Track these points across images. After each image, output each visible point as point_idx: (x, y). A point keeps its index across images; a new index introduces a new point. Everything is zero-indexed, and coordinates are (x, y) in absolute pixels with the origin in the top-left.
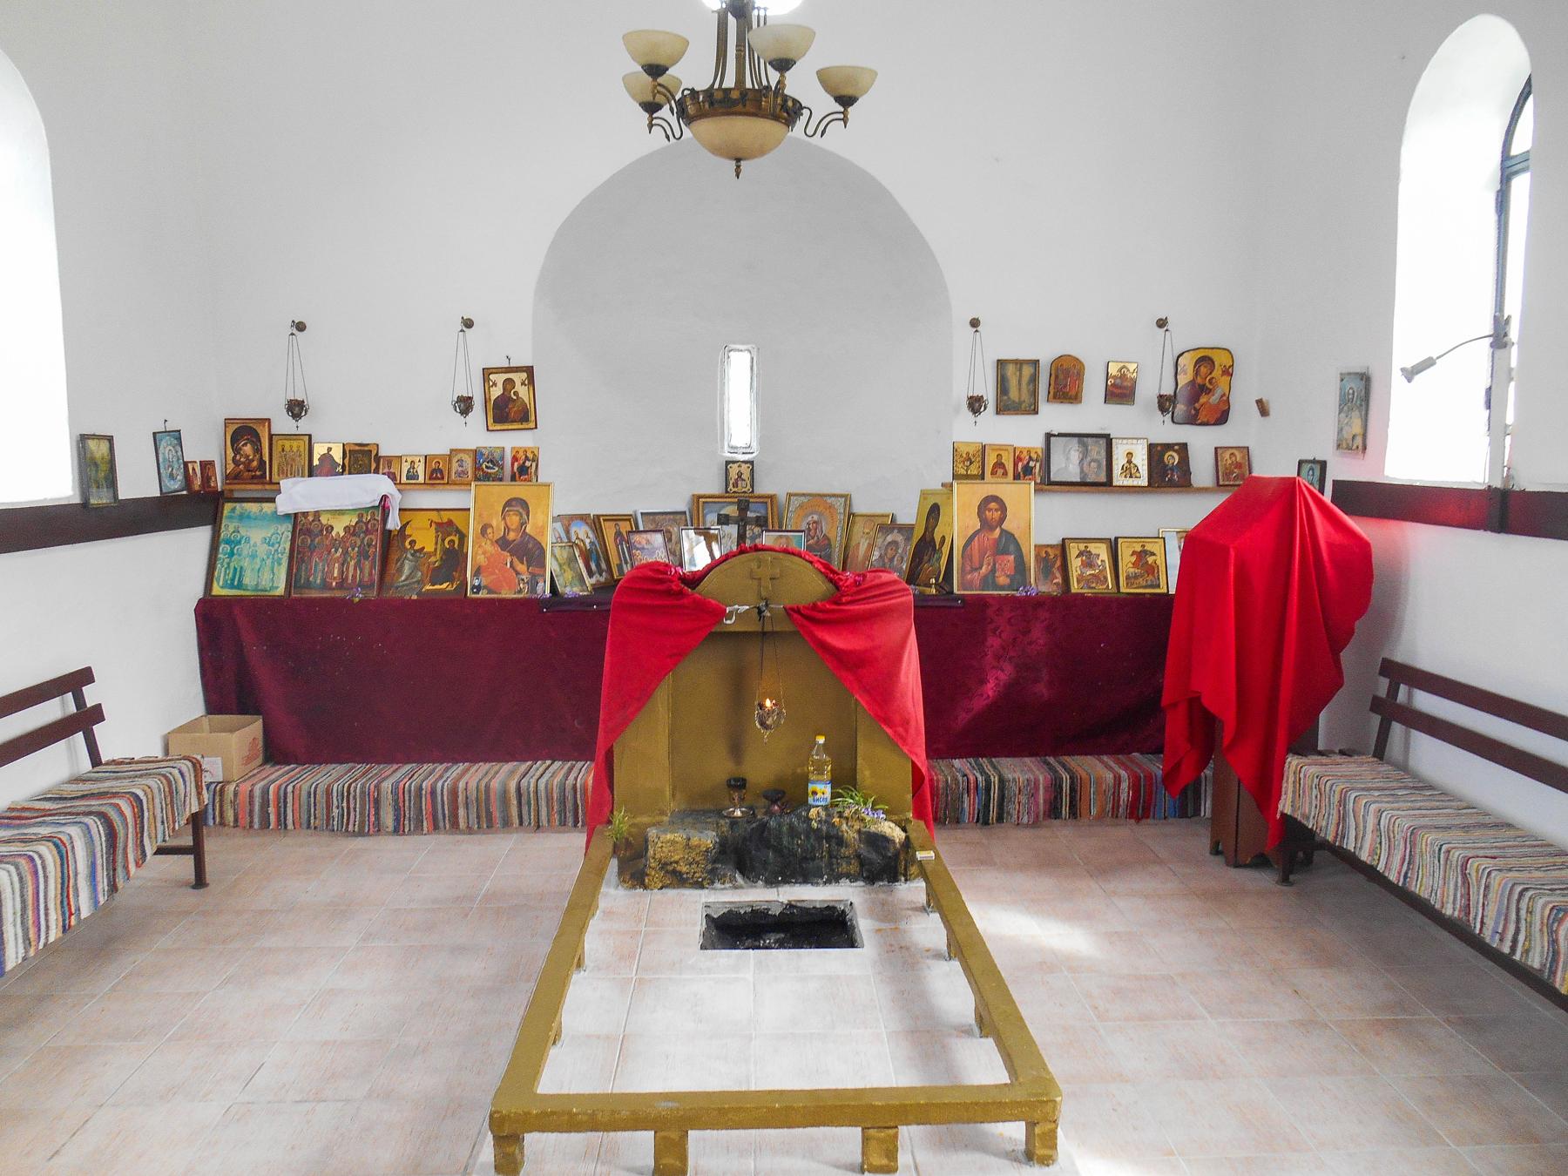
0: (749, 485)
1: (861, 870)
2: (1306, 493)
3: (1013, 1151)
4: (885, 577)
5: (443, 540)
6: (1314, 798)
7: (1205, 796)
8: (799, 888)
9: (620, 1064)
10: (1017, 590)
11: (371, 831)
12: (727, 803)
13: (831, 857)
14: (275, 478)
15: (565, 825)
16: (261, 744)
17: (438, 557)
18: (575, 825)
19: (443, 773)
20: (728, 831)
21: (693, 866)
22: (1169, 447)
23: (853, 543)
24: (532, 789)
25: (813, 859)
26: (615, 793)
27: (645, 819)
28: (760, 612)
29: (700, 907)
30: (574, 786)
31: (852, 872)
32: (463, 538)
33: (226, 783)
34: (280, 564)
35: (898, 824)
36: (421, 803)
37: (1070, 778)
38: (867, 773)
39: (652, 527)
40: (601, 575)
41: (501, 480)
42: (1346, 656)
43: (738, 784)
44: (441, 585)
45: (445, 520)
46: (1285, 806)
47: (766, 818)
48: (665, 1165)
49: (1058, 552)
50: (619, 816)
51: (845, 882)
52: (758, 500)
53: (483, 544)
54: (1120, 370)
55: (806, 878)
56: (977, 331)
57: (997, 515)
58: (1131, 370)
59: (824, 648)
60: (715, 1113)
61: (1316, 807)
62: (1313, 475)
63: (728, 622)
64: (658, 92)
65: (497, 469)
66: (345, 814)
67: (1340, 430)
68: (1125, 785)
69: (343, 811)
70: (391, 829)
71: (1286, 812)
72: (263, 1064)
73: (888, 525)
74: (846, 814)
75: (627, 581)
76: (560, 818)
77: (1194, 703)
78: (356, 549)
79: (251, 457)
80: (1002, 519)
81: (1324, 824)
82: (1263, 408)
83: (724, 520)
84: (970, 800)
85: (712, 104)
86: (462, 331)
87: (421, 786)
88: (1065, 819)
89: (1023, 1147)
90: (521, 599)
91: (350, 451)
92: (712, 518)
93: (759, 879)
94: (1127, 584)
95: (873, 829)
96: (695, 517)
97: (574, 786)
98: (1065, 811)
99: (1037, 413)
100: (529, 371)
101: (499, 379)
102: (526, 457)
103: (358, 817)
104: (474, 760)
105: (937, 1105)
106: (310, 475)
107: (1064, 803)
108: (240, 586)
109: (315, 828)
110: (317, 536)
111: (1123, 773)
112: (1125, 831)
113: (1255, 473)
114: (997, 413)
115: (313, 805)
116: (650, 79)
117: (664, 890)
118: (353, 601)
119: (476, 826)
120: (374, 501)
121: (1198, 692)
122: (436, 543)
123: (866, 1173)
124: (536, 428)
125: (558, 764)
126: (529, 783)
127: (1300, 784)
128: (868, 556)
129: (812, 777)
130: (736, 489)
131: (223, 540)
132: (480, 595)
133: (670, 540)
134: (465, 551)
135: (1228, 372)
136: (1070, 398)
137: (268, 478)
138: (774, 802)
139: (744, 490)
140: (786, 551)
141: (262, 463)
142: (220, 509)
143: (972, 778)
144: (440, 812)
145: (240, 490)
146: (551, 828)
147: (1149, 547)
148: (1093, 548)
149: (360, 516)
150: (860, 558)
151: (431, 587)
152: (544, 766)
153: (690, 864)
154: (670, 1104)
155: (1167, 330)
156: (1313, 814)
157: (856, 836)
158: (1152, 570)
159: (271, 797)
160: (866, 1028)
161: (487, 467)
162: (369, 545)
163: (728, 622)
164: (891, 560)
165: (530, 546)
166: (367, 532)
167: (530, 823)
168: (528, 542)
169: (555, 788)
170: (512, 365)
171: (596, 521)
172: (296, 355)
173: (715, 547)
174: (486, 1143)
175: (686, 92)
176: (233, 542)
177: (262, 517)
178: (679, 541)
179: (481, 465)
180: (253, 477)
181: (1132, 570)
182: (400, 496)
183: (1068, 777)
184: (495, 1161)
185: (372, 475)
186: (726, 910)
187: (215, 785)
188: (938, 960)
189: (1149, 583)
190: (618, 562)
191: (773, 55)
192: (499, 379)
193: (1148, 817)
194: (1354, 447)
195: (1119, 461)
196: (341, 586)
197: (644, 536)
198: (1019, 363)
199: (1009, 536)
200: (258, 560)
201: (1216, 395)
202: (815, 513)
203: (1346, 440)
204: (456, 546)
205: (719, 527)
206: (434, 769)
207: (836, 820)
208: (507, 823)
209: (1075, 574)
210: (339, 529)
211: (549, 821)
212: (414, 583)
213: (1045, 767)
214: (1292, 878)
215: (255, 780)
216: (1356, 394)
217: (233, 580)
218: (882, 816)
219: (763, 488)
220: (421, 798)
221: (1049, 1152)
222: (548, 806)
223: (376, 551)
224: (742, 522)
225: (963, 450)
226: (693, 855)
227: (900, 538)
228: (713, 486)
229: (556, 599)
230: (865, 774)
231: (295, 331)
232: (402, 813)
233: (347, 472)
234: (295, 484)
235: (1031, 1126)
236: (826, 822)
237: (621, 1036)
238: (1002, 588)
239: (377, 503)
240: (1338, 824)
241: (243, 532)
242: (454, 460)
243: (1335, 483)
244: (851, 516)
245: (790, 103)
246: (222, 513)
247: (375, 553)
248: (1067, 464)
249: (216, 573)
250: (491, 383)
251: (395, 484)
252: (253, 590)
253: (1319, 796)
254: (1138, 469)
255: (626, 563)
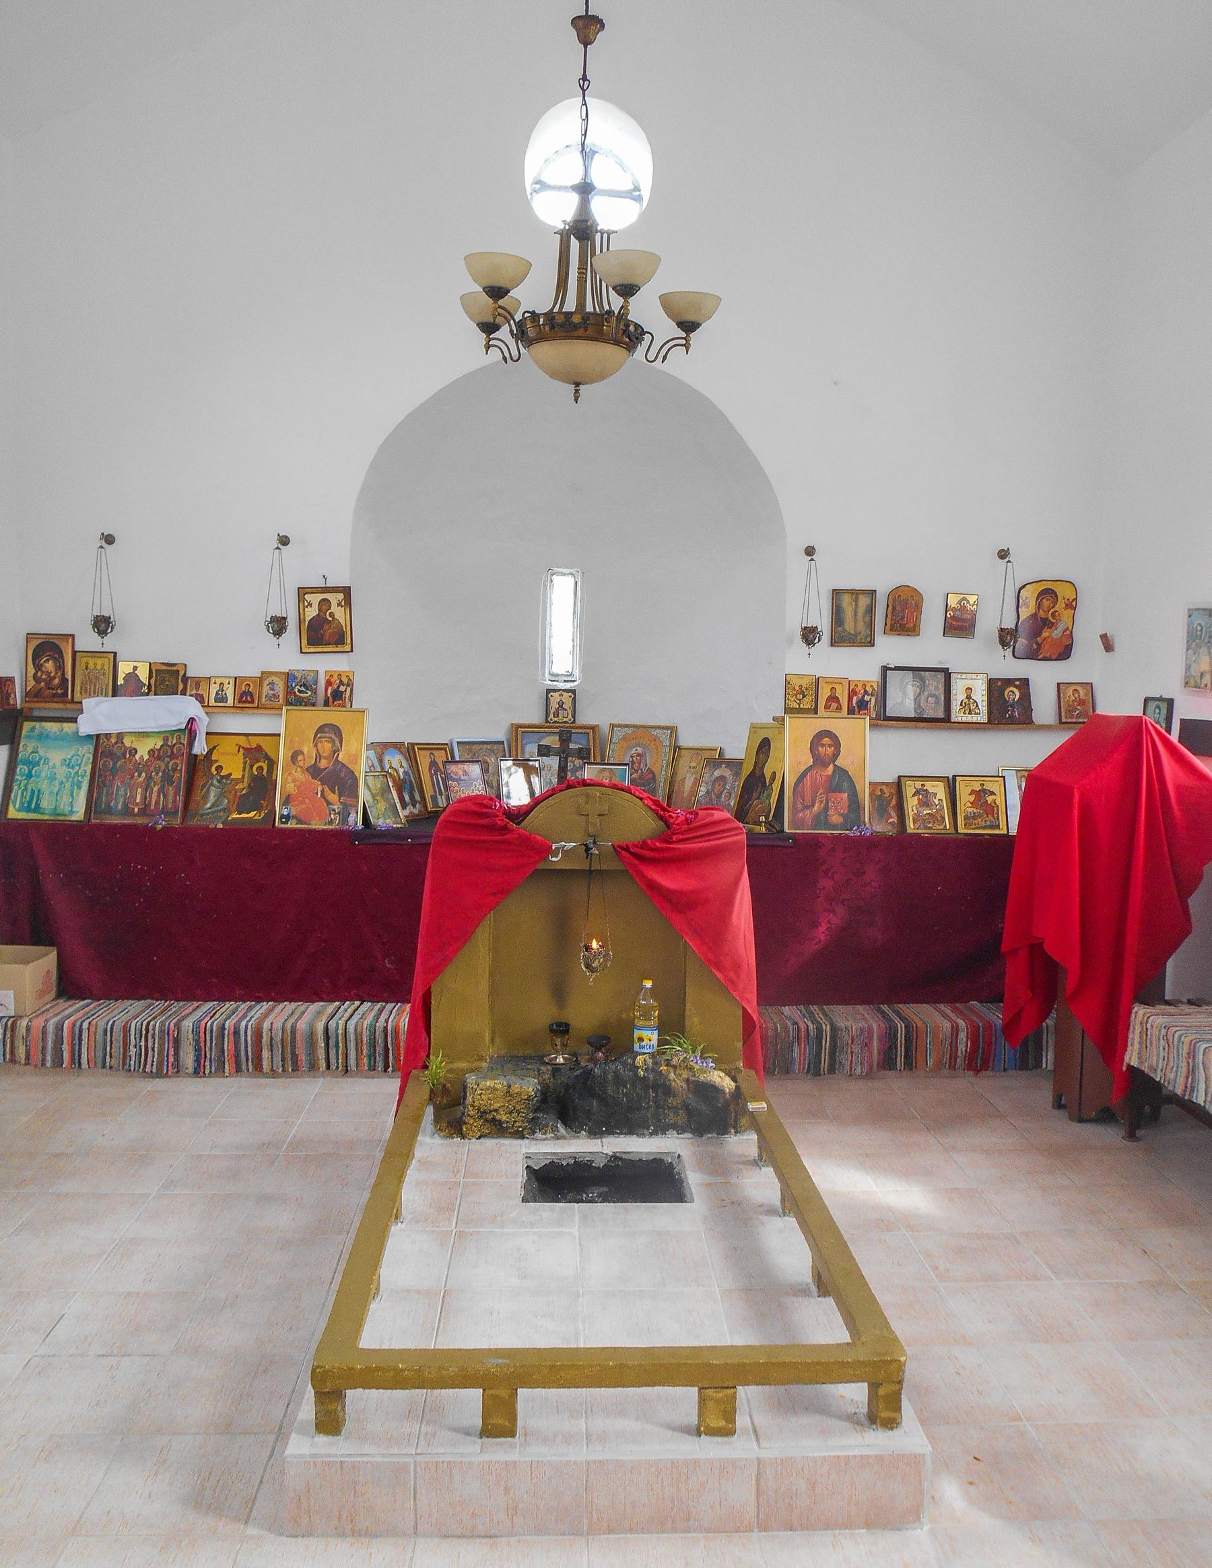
0: (570, 713)
1: (689, 1122)
2: (1153, 732)
3: (855, 1413)
4: (718, 815)
5: (251, 767)
6: (1161, 1048)
7: (1047, 1048)
8: (625, 1139)
9: (442, 1321)
10: (851, 829)
11: (170, 1073)
12: (549, 1047)
13: (658, 1107)
14: (77, 697)
15: (374, 1070)
16: (54, 977)
17: (246, 784)
18: (386, 1071)
19: (246, 1012)
20: (549, 1079)
21: (513, 1115)
22: (1009, 682)
23: (679, 778)
24: (340, 1031)
25: (639, 1109)
26: (432, 1036)
27: (462, 1065)
28: (588, 849)
29: (520, 1157)
30: (385, 1028)
31: (680, 1123)
32: (272, 764)
33: (18, 1017)
34: (79, 788)
35: (728, 1073)
36: (223, 1044)
37: (905, 1027)
38: (696, 1020)
39: (468, 757)
40: (414, 806)
41: (313, 705)
42: (1194, 902)
43: (561, 1029)
44: (248, 813)
45: (254, 746)
46: (1132, 1058)
47: (591, 1065)
48: (493, 1425)
49: (893, 791)
50: (437, 1063)
51: (672, 1134)
52: (580, 731)
53: (293, 772)
54: (960, 602)
55: (631, 1127)
56: (812, 560)
57: (830, 751)
58: (972, 602)
59: (652, 887)
60: (546, 1371)
61: (1164, 1059)
62: (1159, 713)
63: (554, 859)
64: (499, 314)
65: (310, 693)
66: (143, 1053)
67: (1188, 668)
68: (963, 1036)
69: (141, 1050)
70: (191, 1070)
71: (1132, 1064)
72: (63, 1315)
73: (715, 759)
74: (675, 1061)
75: (450, 815)
76: (370, 1062)
77: (1036, 949)
78: (160, 774)
79: (52, 675)
80: (836, 755)
81: (1172, 1076)
82: (1108, 644)
83: (544, 751)
84: (800, 1048)
85: (552, 327)
86: (278, 548)
87: (224, 1025)
88: (900, 1070)
89: (865, 1410)
90: (331, 830)
91: (156, 670)
92: (531, 749)
93: (582, 1129)
94: (965, 825)
95: (702, 1078)
96: (513, 748)
97: (385, 1028)
98: (900, 1061)
99: (873, 645)
100: (346, 591)
101: (315, 599)
102: (341, 681)
103: (156, 1056)
104: (278, 999)
105: (778, 1365)
106: (114, 695)
107: (899, 1053)
108: (37, 809)
109: (111, 1068)
110: (119, 759)
111: (961, 1023)
112: (965, 1083)
113: (1099, 711)
114: (832, 645)
115: (108, 1044)
116: (491, 301)
117: (482, 1140)
118: (155, 828)
119: (281, 1069)
120: (181, 723)
121: (1041, 939)
122: (244, 770)
123: (703, 1436)
124: (352, 651)
125: (367, 1005)
126: (337, 1024)
127: (1147, 1035)
128: (694, 792)
129: (639, 1023)
130: (556, 719)
131: (21, 761)
132: (289, 825)
133: (487, 771)
134: (274, 778)
135: (1071, 605)
136: (908, 630)
137: (69, 697)
138: (599, 1049)
139: (565, 720)
140: (615, 787)
141: (64, 680)
142: (19, 725)
143: (802, 1026)
144: (243, 1053)
145: (40, 709)
146: (359, 1072)
147: (988, 786)
148: (930, 786)
149: (166, 739)
150: (686, 794)
151: (238, 816)
152: (353, 1007)
153: (511, 1113)
154: (500, 1361)
155: (1009, 561)
156: (1160, 1067)
157: (684, 1085)
158: (991, 810)
159: (65, 1034)
160: (698, 1286)
161: (299, 691)
162: (174, 770)
163: (554, 859)
164: (719, 796)
165: (342, 775)
166: (172, 756)
167: (337, 1068)
168: (340, 770)
169: (365, 1030)
170: (328, 585)
171: (410, 749)
172: (104, 566)
173: (535, 780)
174: (305, 1401)
175: (527, 315)
176: (31, 762)
177: (62, 738)
178: (498, 773)
179: (293, 689)
180: (54, 695)
181: (970, 810)
182: (208, 719)
183: (903, 1025)
184: (316, 1418)
185: (179, 696)
186: (547, 1162)
187: (6, 1020)
188: (772, 1216)
189: (988, 823)
190: (433, 794)
191: (618, 281)
192: (315, 599)
193: (986, 1070)
194: (1202, 685)
195: (958, 696)
196: (144, 811)
197: (461, 766)
198: (855, 593)
199: (842, 772)
200: (57, 783)
201: (1059, 630)
202: (638, 745)
203: (1194, 677)
204: (265, 771)
205: (539, 758)
206: (236, 1009)
207: (663, 1068)
208: (313, 1067)
209: (911, 813)
210: (143, 753)
211: (357, 1066)
212: (220, 811)
213: (879, 1015)
214: (1139, 1133)
215: (50, 1014)
216: (1204, 631)
217: (30, 802)
218: (711, 1065)
219: (586, 717)
220: (224, 1038)
221: (893, 1415)
222: (357, 1049)
223: (181, 776)
224: (564, 753)
225: (796, 682)
226: (513, 1103)
227: (727, 773)
228: (533, 716)
229: (368, 831)
230: (693, 1020)
231: (104, 544)
232: (203, 1054)
233: (153, 692)
234: (98, 704)
235: (874, 1387)
236: (653, 1070)
237: (442, 1292)
238: (835, 827)
239: (183, 726)
240: (1187, 1078)
241: (42, 752)
242: (266, 683)
243: (1182, 720)
244: (678, 748)
245: (632, 328)
246: (21, 733)
247: (180, 778)
248: (902, 699)
249: (13, 795)
250: (306, 604)
251: (202, 706)
252: (51, 815)
253: (1167, 1048)
254: (977, 706)
255: (441, 794)
